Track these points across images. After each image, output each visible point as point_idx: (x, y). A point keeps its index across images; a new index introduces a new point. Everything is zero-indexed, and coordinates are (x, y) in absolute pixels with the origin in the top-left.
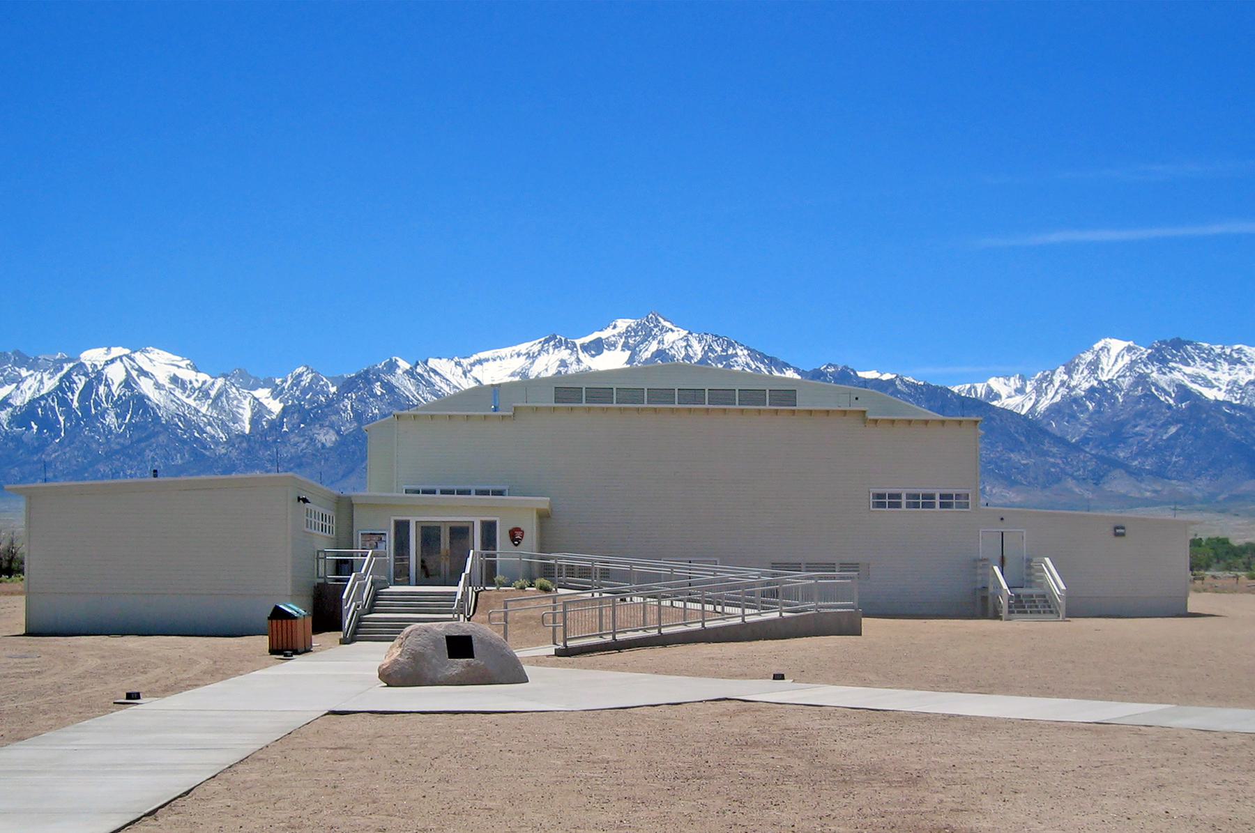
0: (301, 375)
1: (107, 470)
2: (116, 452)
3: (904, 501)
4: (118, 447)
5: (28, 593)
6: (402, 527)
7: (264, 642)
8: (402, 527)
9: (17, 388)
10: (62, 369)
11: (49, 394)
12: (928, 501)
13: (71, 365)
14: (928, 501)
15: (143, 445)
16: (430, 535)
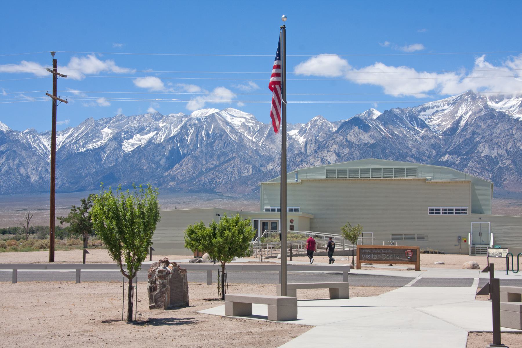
0: (316, 121)
1: (206, 179)
2: (211, 169)
3: (441, 211)
4: (213, 166)
5: (225, 304)
6: (256, 222)
7: (326, 292)
8: (256, 222)
9: (157, 134)
10: (182, 121)
11: (174, 137)
12: (451, 212)
13: (186, 119)
14: (451, 212)
15: (226, 165)
16: (264, 224)
